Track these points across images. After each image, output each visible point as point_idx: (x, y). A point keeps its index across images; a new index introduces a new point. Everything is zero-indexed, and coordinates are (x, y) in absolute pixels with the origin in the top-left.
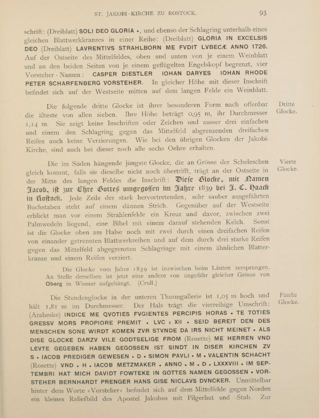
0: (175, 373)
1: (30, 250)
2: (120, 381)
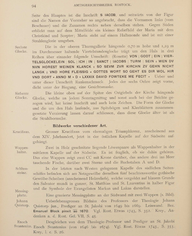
0: (101, 72)
1: (85, 195)
2: (41, 72)
